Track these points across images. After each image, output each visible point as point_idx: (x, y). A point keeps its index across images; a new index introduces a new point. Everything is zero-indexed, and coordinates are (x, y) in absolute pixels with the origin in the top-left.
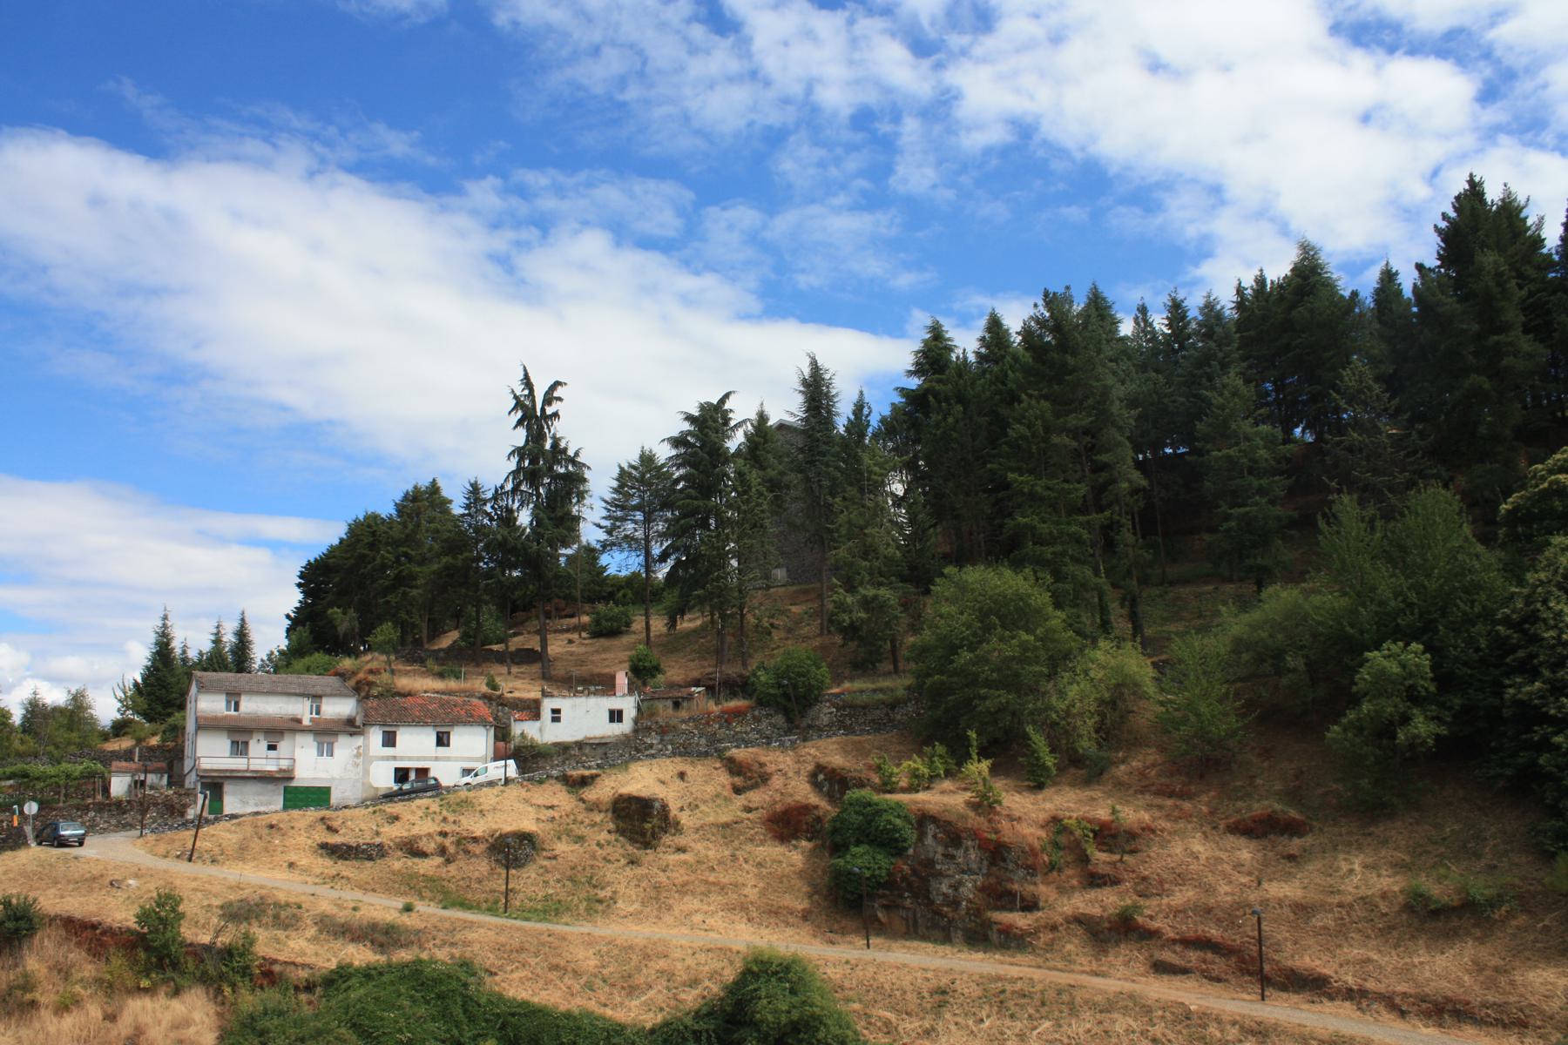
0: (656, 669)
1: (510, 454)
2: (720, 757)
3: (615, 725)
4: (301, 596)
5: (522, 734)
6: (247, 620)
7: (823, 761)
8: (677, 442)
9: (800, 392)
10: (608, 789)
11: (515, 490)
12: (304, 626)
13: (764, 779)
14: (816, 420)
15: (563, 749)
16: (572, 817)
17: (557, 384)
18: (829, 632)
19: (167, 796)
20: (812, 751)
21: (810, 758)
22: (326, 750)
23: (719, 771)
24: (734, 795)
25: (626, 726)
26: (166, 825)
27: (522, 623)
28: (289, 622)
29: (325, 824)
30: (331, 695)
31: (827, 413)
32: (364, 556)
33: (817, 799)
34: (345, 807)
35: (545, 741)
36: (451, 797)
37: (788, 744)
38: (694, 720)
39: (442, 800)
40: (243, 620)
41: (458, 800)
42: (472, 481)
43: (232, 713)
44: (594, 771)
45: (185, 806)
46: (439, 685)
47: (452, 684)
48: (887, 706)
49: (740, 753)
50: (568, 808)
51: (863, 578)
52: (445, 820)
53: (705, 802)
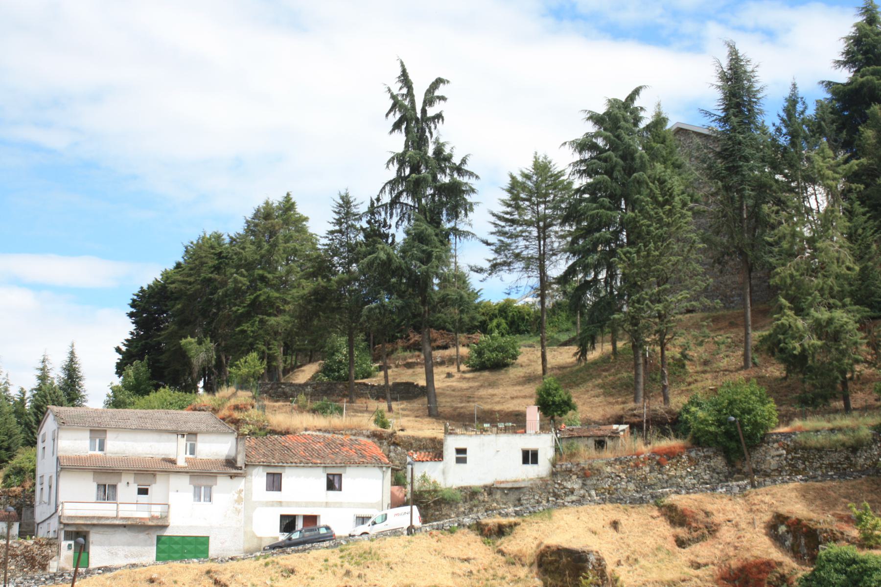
0: (566, 405)
1: (389, 162)
2: (657, 504)
3: (530, 467)
4: (132, 327)
5: (423, 476)
6: (77, 354)
7: (783, 510)
8: (582, 146)
9: (719, 87)
10: (530, 540)
11: (395, 202)
12: (142, 360)
13: (712, 530)
14: (738, 119)
15: (471, 494)
16: (491, 571)
17: (439, 82)
18: (755, 364)
19: (26, 547)
20: (767, 499)
21: (764, 507)
22: (204, 494)
23: (658, 520)
24: (677, 548)
25: (542, 468)
26: (32, 578)
27: (388, 355)
28: (120, 357)
29: (211, 577)
30: (208, 432)
31: (749, 111)
32: (210, 280)
33: (780, 555)
34: (232, 559)
35: (448, 485)
36: (353, 548)
37: (737, 490)
38: (621, 463)
39: (342, 551)
40: (72, 353)
41: (361, 551)
42: (343, 194)
43: (97, 452)
44: (512, 520)
45: (47, 558)
46: (320, 421)
47: (336, 421)
48: (847, 448)
49: (682, 501)
50: (486, 562)
51: (815, 298)
52: (348, 573)
53: (645, 556)
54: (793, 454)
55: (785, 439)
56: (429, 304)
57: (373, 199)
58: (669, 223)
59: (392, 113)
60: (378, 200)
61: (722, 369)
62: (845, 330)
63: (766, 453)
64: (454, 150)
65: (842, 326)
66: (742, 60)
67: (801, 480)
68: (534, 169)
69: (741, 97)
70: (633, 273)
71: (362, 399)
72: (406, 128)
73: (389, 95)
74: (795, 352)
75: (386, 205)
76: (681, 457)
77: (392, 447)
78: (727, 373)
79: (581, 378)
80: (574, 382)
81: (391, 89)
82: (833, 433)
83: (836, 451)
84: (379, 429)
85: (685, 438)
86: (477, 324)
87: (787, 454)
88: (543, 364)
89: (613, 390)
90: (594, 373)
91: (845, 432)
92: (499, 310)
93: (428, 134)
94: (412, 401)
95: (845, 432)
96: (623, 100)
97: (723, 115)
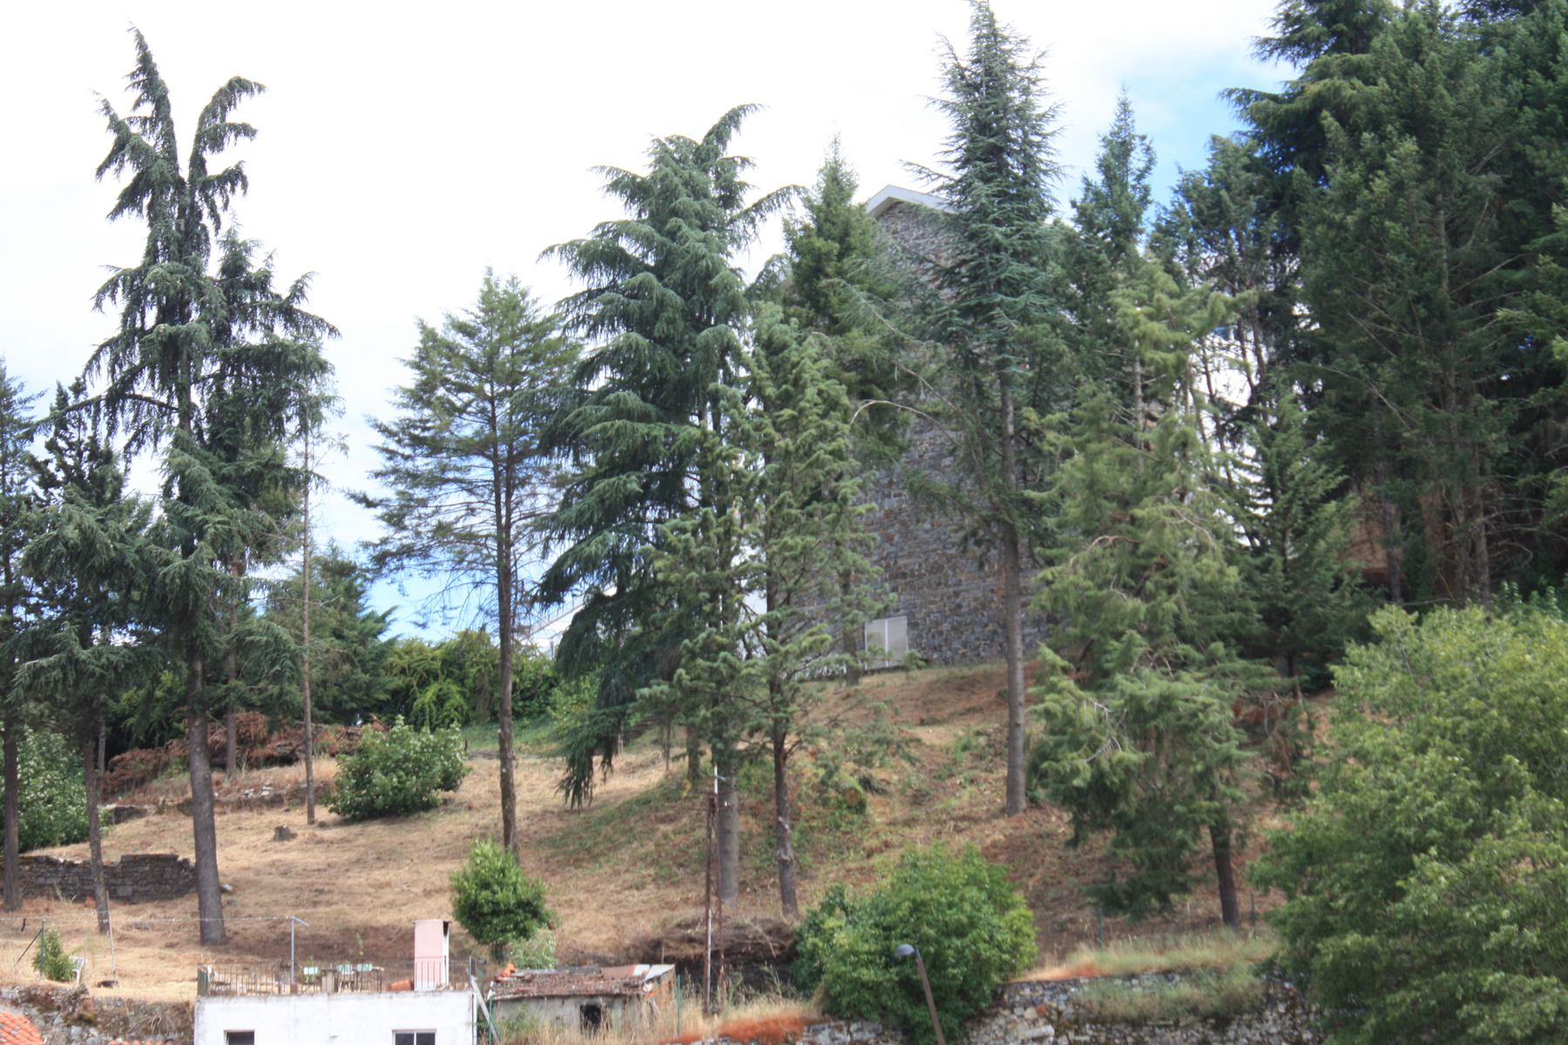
0: (528, 913)
1: (102, 291)
8: (590, 256)
11: (117, 396)
14: (993, 188)
17: (237, 87)
48: (1204, 1019)
54: (1071, 1035)
55: (1052, 997)
56: (204, 657)
57: (66, 388)
58: (787, 452)
59: (115, 166)
60: (78, 388)
61: (955, 814)
62: (1201, 723)
63: (1006, 1032)
64: (276, 261)
65: (1194, 715)
66: (1005, 39)
68: (483, 310)
69: (1003, 132)
70: (690, 581)
71: (39, 899)
72: (151, 207)
73: (107, 120)
74: (1077, 782)
75: (97, 402)
77: (75, 1030)
78: (963, 825)
79: (608, 839)
80: (588, 851)
81: (112, 105)
82: (1170, 980)
83: (1176, 1025)
84: (45, 982)
85: (808, 997)
86: (383, 697)
88: (504, 805)
89: (681, 872)
90: (639, 827)
91: (1199, 977)
92: (444, 662)
93: (207, 221)
94: (169, 904)
95: (1199, 977)
96: (699, 139)
97: (957, 176)
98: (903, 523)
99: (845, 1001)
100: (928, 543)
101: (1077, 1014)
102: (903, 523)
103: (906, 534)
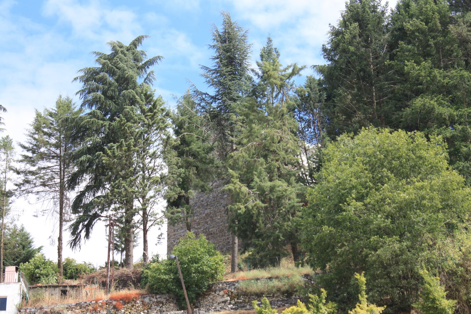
54: (236, 300)
55: (229, 287)
67: (232, 309)
76: (135, 302)
82: (271, 281)
87: (230, 300)
98: (211, 217)
99: (155, 287)
100: (219, 223)
101: (238, 293)
102: (211, 217)
103: (212, 220)
